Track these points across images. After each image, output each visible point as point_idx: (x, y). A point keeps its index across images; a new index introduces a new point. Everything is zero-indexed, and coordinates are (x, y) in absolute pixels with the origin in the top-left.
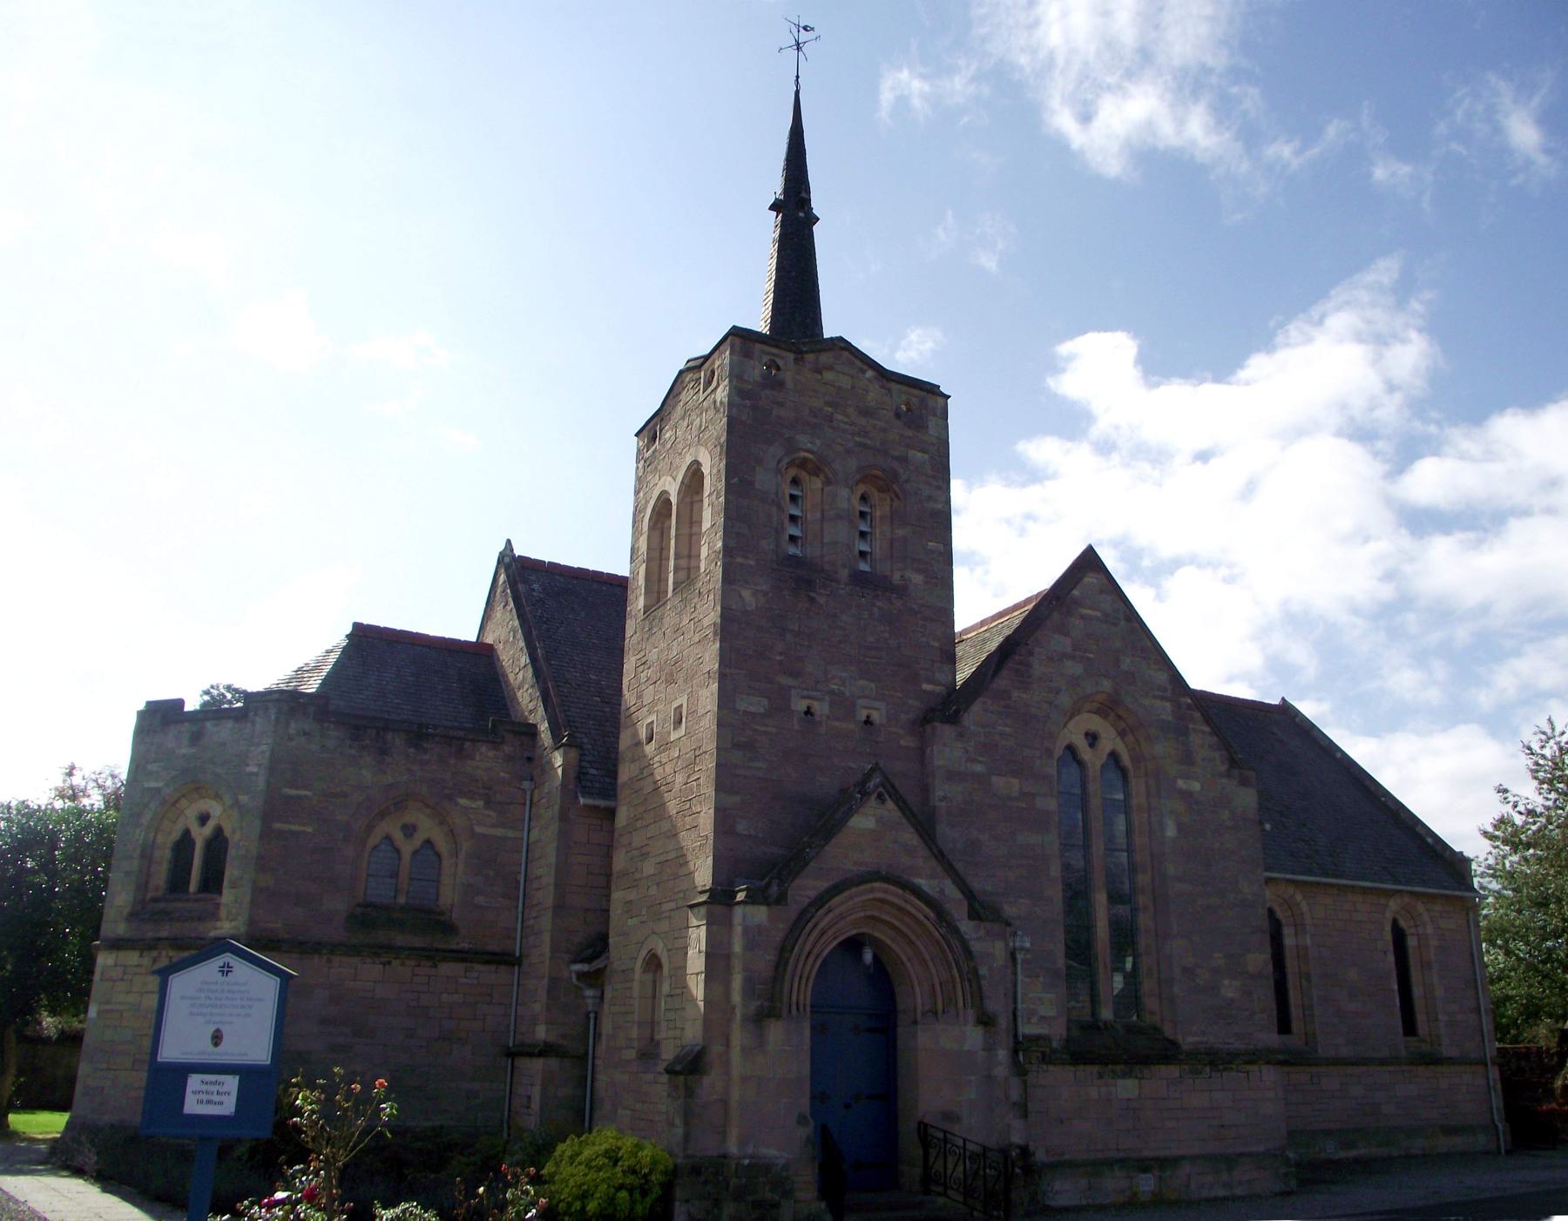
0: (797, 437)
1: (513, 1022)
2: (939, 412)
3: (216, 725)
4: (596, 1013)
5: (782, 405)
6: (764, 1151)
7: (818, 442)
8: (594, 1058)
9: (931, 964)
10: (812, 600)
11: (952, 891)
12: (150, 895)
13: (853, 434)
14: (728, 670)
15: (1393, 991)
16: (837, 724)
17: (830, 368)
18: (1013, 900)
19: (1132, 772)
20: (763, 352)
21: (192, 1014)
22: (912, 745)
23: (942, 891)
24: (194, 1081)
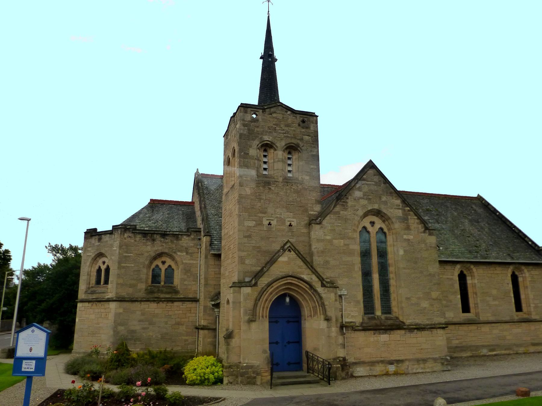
0: (264, 137)
1: (198, 318)
2: (314, 122)
3: (105, 236)
4: (219, 316)
5: (258, 127)
6: (250, 361)
7: (271, 138)
8: (218, 329)
9: (309, 301)
10: (270, 189)
11: (314, 278)
12: (90, 286)
13: (283, 133)
14: (241, 214)
15: (511, 297)
16: (279, 227)
17: (275, 112)
18: (341, 279)
19: (388, 234)
20: (252, 111)
21: (25, 343)
22: (306, 232)
23: (311, 279)
24: (24, 361)
